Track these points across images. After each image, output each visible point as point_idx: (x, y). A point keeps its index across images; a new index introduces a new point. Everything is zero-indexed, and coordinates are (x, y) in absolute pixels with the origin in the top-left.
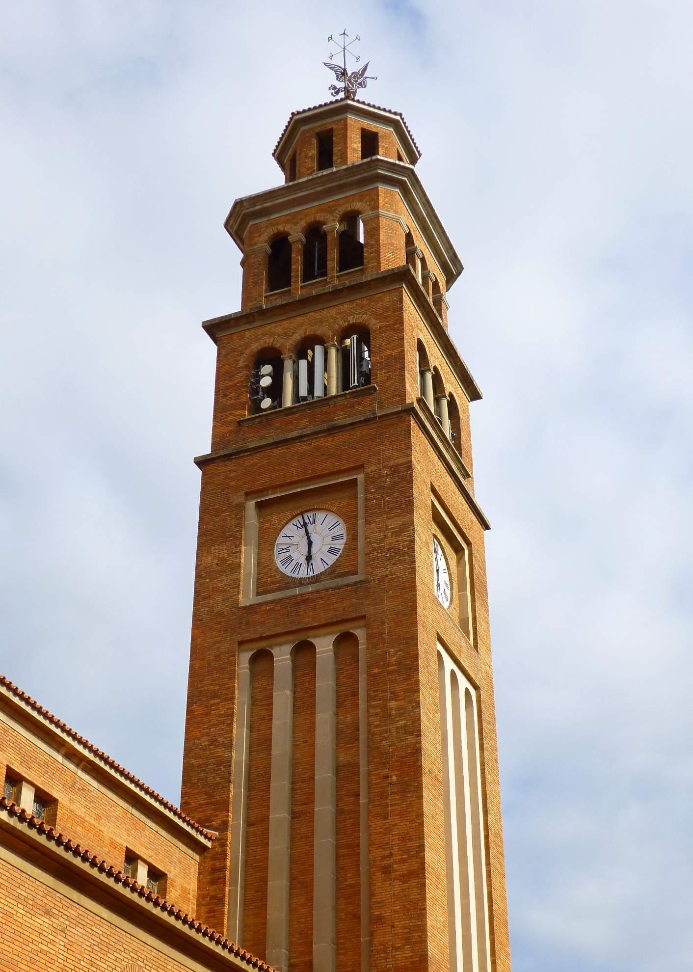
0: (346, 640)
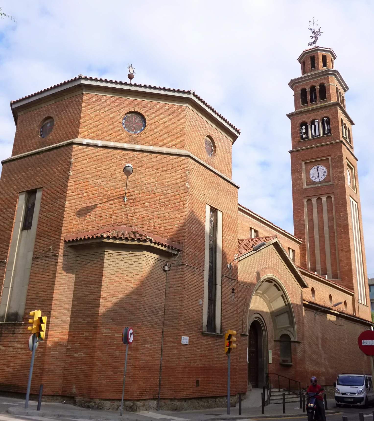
0: (329, 197)
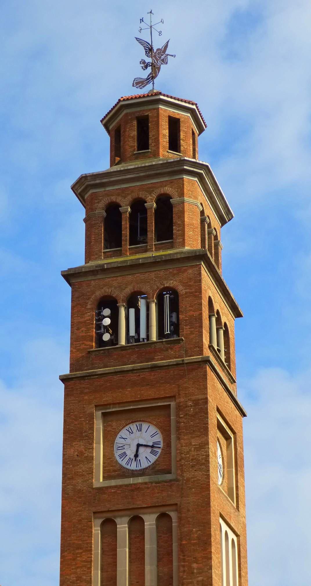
0: (163, 517)
